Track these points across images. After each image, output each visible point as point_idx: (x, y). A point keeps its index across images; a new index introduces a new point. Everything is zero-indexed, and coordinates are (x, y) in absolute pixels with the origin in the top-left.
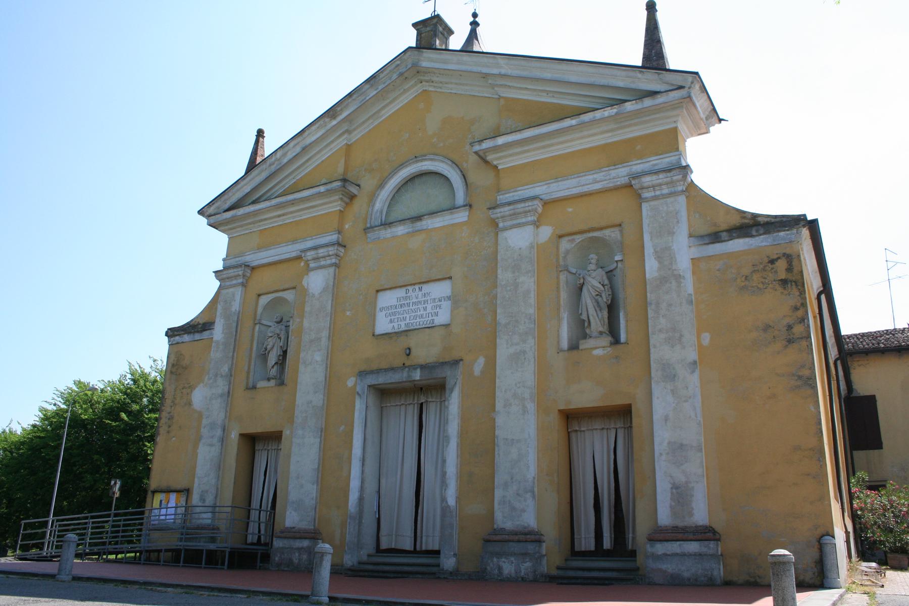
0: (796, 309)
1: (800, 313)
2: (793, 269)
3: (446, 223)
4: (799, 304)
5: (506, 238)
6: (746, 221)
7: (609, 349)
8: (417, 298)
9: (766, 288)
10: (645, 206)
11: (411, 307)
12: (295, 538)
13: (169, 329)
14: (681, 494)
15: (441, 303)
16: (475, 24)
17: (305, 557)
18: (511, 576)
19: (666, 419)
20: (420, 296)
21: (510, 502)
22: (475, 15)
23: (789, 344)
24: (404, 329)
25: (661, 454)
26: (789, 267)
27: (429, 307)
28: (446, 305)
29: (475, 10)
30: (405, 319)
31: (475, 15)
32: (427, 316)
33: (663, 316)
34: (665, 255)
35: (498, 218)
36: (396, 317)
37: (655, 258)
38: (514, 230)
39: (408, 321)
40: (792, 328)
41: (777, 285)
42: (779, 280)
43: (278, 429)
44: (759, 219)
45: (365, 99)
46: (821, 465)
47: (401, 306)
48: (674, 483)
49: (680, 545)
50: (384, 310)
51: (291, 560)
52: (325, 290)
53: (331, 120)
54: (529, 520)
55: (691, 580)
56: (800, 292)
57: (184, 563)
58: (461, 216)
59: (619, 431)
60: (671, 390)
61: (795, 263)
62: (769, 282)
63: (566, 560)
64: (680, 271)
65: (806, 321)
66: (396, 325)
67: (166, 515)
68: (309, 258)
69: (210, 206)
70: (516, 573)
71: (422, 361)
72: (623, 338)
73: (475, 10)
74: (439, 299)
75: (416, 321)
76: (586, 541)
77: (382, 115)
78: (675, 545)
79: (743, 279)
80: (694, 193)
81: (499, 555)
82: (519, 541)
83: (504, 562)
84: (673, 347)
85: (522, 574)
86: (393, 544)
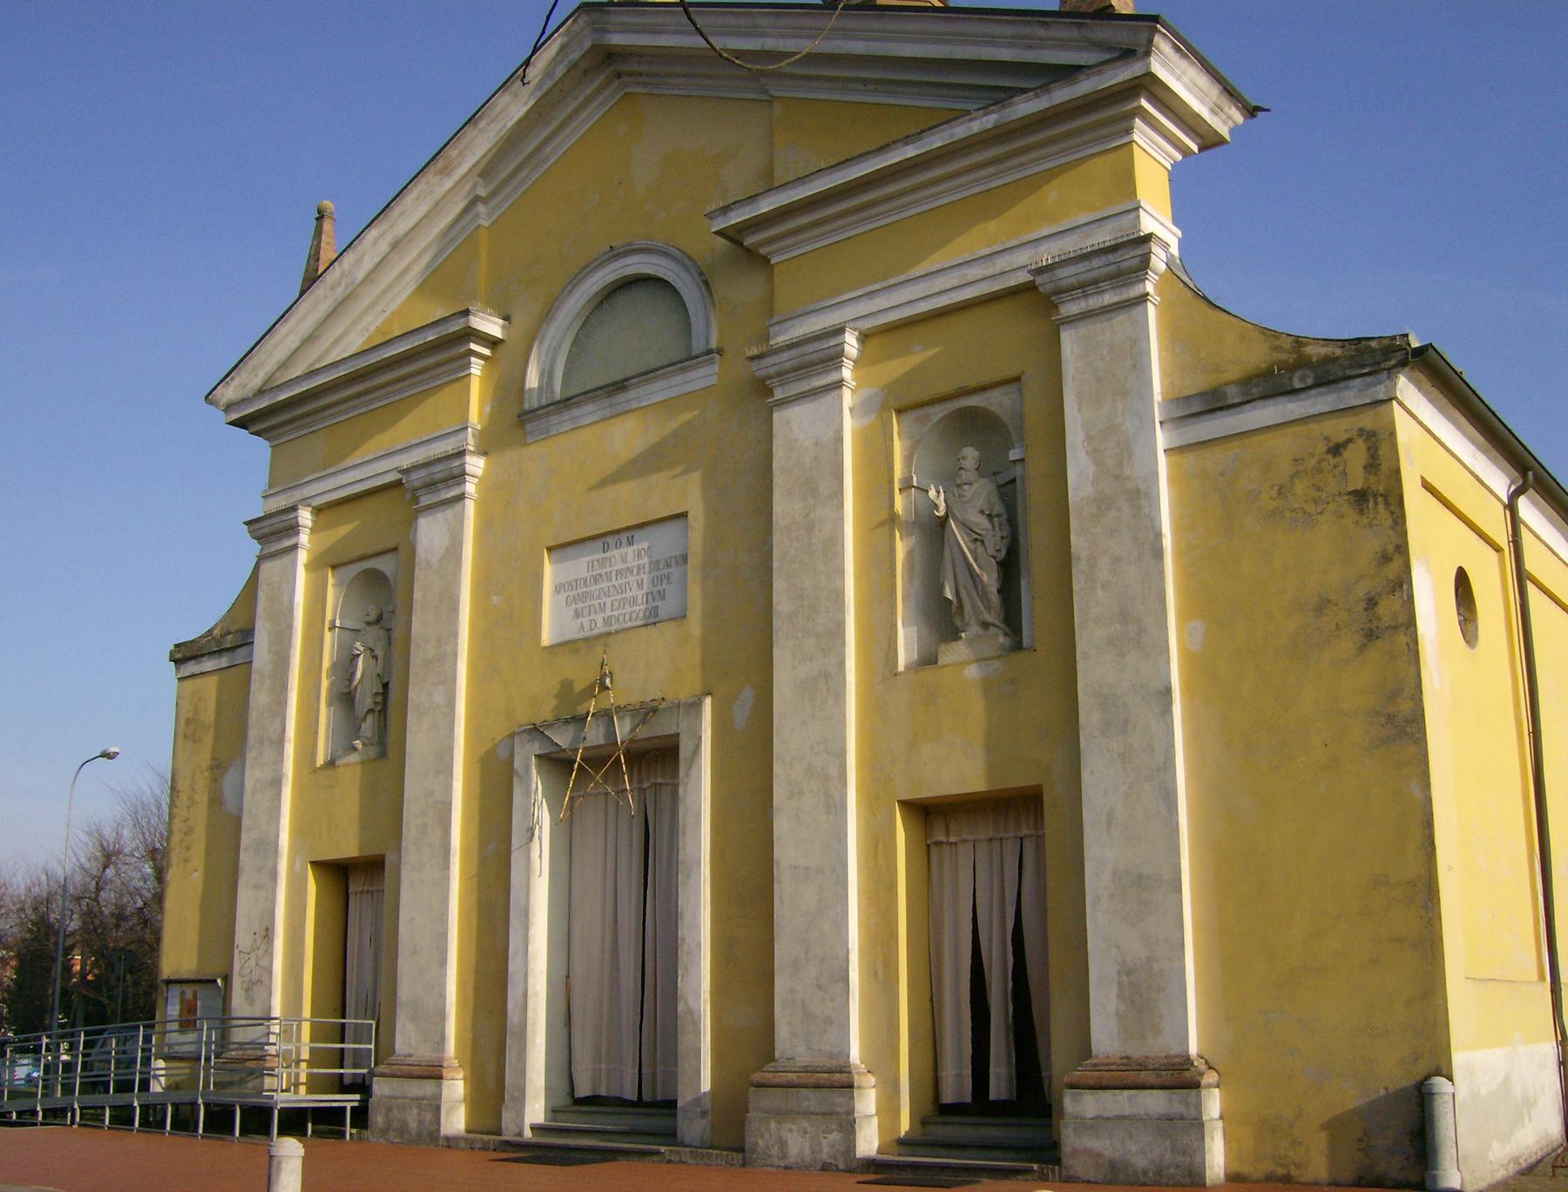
0: (1385, 558)
1: (1393, 569)
2: (1380, 464)
3: (674, 392)
4: (1391, 548)
5: (788, 422)
6: (1283, 356)
7: (996, 664)
8: (624, 561)
9: (1321, 513)
11: (614, 582)
13: (177, 646)
15: (669, 570)
18: (802, 1159)
20: (630, 556)
21: (803, 1002)
23: (1370, 640)
24: (602, 630)
25: (1098, 898)
26: (1371, 461)
30: (602, 608)
32: (645, 599)
33: (1103, 586)
35: (770, 378)
36: (586, 604)
37: (1087, 453)
39: (609, 613)
40: (1375, 604)
41: (1346, 505)
42: (1350, 493)
43: (382, 853)
45: (504, 126)
46: (1430, 920)
47: (595, 580)
48: (1125, 961)
49: (1130, 1098)
50: (562, 590)
51: (405, 1123)
53: (442, 179)
55: (1151, 1174)
56: (1394, 520)
57: (345, 1108)
59: (1027, 843)
60: (1119, 755)
61: (1383, 452)
62: (1328, 497)
63: (924, 1123)
64: (1139, 482)
65: (1405, 586)
66: (586, 621)
68: (417, 484)
69: (227, 383)
70: (813, 1153)
71: (635, 698)
72: (1026, 641)
74: (666, 561)
75: (625, 611)
76: (958, 1085)
77: (547, 157)
78: (1119, 1098)
79: (1274, 493)
81: (781, 1115)
82: (817, 1086)
83: (791, 1130)
84: (1122, 655)
85: (825, 1156)
86: (603, 1084)
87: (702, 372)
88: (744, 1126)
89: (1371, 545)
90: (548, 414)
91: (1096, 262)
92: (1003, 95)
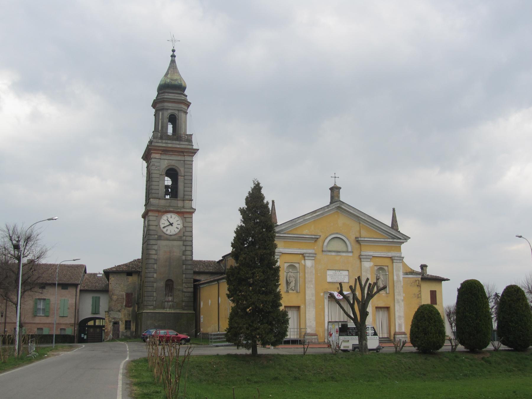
10: (394, 263)
12: (312, 336)
14: (400, 326)
16: (173, 56)
17: (316, 340)
19: (398, 311)
22: (173, 51)
27: (342, 277)
28: (347, 277)
29: (174, 47)
31: (173, 51)
34: (398, 276)
38: (366, 262)
44: (414, 271)
52: (312, 266)
54: (403, 330)
58: (351, 254)
67: (297, 329)
73: (174, 47)
80: (405, 265)
87: (351, 254)
88: (506, 346)
89: (419, 290)
90: (327, 252)
91: (399, 258)
92: (394, 238)
